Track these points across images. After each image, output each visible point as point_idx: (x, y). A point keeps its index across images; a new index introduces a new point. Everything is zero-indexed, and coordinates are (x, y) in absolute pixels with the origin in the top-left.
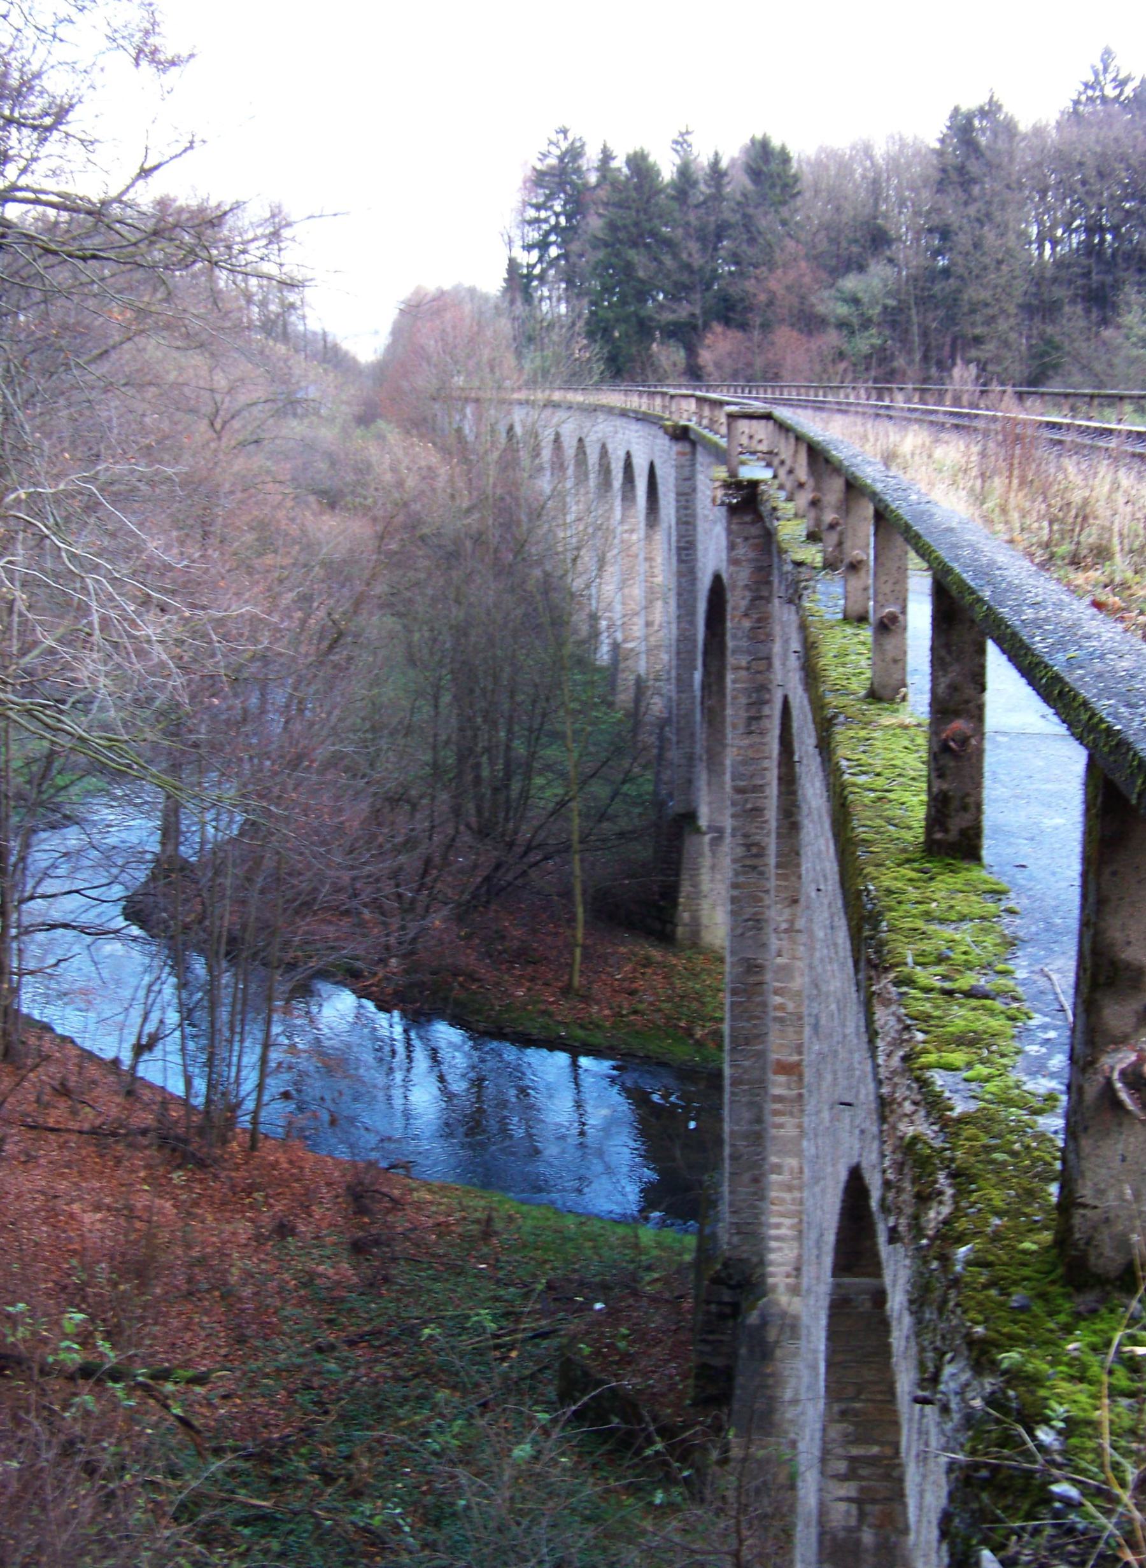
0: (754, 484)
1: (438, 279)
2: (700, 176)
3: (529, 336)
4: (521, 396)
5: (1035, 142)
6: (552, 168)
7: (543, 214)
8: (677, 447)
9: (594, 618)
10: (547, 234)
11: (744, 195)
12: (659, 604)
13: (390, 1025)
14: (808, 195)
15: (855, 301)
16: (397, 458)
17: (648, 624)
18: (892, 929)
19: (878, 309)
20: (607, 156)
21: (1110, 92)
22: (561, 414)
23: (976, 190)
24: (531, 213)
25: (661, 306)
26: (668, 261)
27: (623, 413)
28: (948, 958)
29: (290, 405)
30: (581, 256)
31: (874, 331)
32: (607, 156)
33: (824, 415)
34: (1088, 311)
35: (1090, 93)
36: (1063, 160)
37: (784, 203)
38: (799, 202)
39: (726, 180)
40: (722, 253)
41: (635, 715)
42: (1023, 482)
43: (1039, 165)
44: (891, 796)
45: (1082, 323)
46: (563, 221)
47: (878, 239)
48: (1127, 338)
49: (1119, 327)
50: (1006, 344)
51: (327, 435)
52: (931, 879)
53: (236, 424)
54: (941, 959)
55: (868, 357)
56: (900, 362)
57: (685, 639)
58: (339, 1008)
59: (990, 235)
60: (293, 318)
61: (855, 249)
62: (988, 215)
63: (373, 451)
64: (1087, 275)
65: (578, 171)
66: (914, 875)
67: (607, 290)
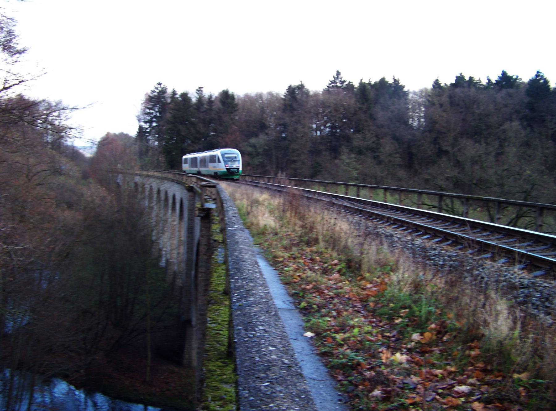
0: (209, 209)
1: (116, 130)
2: (205, 102)
3: (144, 152)
4: (138, 172)
5: (315, 98)
6: (155, 96)
7: (152, 111)
8: (189, 194)
9: (160, 250)
10: (152, 118)
11: (219, 109)
12: (182, 247)
13: (80, 394)
14: (240, 111)
15: (254, 146)
16: (93, 192)
17: (178, 253)
18: (208, 386)
19: (262, 150)
20: (174, 93)
21: (339, 84)
22: (152, 180)
23: (295, 113)
24: (148, 111)
25: (189, 145)
26: (192, 130)
27: (173, 181)
28: (224, 398)
29: (58, 172)
30: (163, 126)
31: (260, 157)
32: (174, 93)
33: (238, 185)
34: (330, 154)
35: (333, 84)
36: (324, 105)
37: (232, 113)
38: (237, 113)
39: (214, 104)
40: (211, 128)
41: (173, 283)
42: (296, 213)
43: (315, 106)
44: (221, 332)
45: (329, 158)
46: (158, 114)
47: (263, 127)
48: (343, 163)
49: (340, 159)
50: (304, 163)
51: (71, 182)
52: (227, 366)
53: (36, 177)
54: (221, 399)
55: (258, 165)
56: (268, 168)
57: (189, 259)
58: (61, 388)
59: (299, 127)
60: (62, 141)
61: (255, 130)
62: (299, 121)
63: (85, 190)
64: (331, 142)
65: (164, 98)
66: (220, 364)
67: (172, 138)
